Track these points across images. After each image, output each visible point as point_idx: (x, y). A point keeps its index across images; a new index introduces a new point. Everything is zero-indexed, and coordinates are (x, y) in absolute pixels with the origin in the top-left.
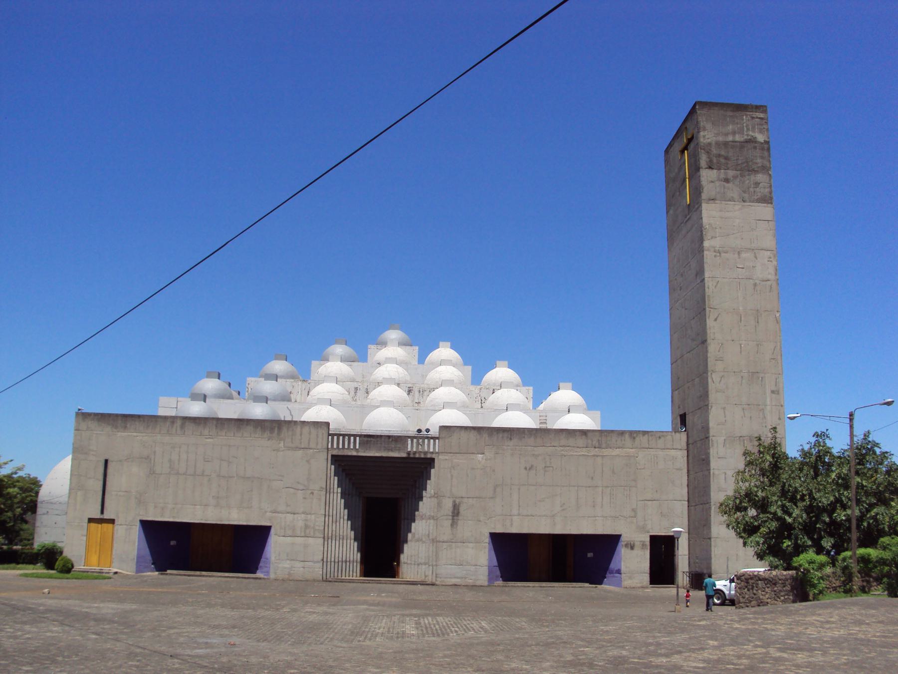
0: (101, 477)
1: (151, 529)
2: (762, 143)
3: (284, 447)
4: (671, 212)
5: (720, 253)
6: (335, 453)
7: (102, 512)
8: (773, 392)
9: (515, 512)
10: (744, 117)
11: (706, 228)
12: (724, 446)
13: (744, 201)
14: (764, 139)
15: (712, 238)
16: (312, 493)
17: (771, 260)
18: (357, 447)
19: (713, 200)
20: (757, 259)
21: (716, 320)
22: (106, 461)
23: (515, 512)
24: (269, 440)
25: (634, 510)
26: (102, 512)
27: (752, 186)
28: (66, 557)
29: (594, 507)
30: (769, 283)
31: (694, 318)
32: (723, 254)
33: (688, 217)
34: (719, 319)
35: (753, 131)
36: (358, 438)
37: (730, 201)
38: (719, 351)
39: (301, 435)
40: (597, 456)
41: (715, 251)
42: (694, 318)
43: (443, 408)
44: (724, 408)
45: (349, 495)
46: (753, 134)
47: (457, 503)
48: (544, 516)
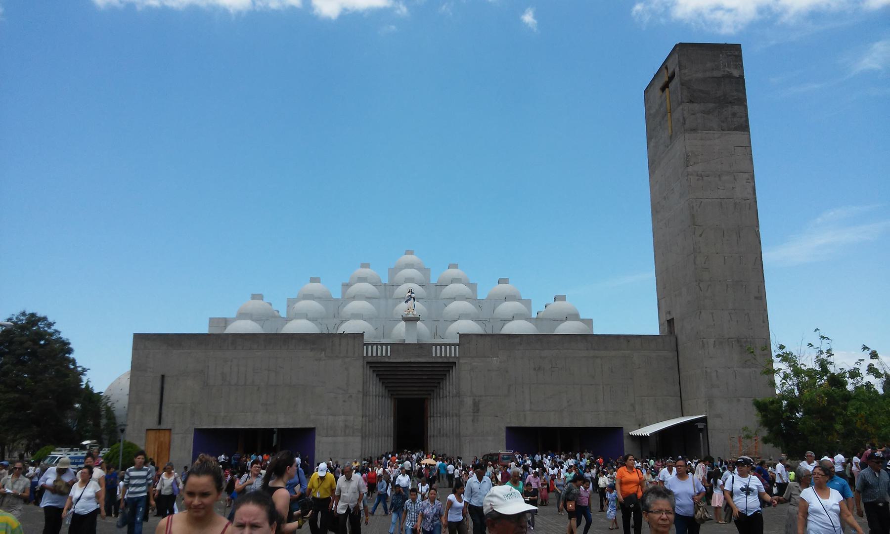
0: (158, 392)
1: (201, 434)
2: (738, 78)
3: (326, 356)
4: (652, 144)
5: (702, 177)
6: (370, 360)
7: (160, 423)
8: (756, 298)
9: (527, 407)
10: (721, 55)
11: (689, 155)
12: (714, 347)
13: (723, 130)
14: (739, 74)
15: (695, 163)
16: (351, 396)
17: (749, 181)
18: (389, 355)
19: (694, 130)
20: (736, 181)
21: (701, 236)
22: (163, 376)
23: (527, 407)
24: (311, 351)
25: (633, 405)
26: (160, 423)
27: (730, 116)
28: (27, 504)
29: (596, 402)
30: (748, 201)
31: (678, 235)
32: (705, 178)
33: (670, 147)
34: (703, 235)
35: (729, 66)
36: (389, 347)
37: (710, 130)
38: (705, 263)
39: (340, 345)
40: (597, 357)
41: (697, 175)
42: (678, 235)
43: (459, 319)
44: (712, 313)
45: (376, 396)
46: (729, 70)
47: (477, 401)
48: (553, 411)
